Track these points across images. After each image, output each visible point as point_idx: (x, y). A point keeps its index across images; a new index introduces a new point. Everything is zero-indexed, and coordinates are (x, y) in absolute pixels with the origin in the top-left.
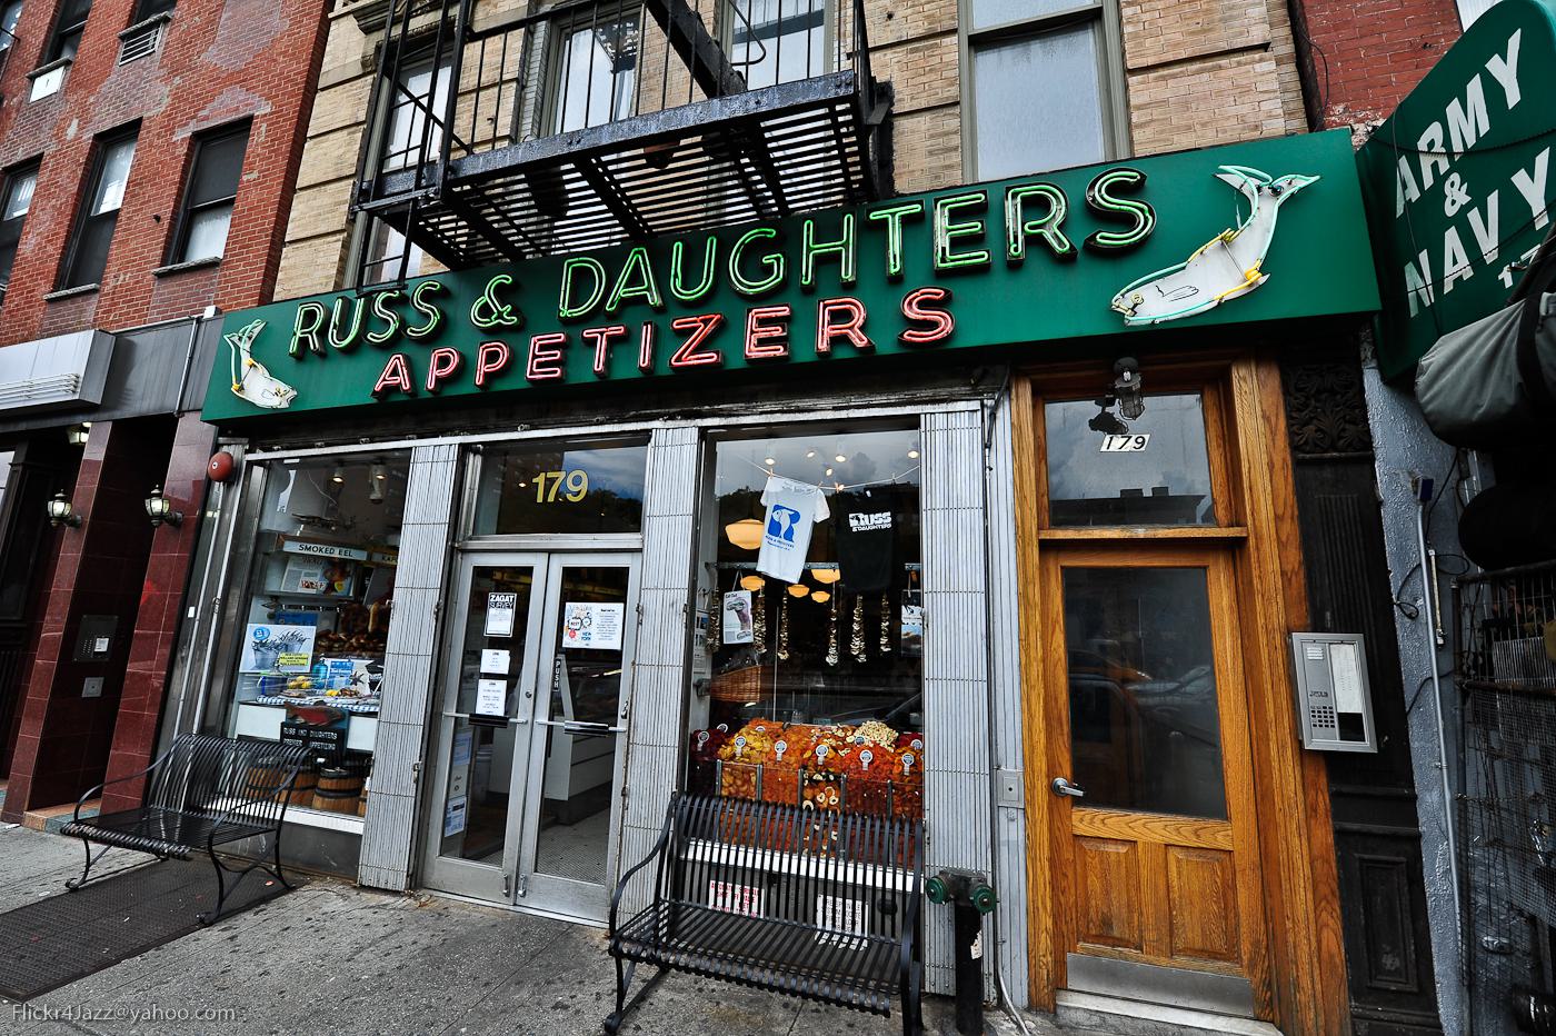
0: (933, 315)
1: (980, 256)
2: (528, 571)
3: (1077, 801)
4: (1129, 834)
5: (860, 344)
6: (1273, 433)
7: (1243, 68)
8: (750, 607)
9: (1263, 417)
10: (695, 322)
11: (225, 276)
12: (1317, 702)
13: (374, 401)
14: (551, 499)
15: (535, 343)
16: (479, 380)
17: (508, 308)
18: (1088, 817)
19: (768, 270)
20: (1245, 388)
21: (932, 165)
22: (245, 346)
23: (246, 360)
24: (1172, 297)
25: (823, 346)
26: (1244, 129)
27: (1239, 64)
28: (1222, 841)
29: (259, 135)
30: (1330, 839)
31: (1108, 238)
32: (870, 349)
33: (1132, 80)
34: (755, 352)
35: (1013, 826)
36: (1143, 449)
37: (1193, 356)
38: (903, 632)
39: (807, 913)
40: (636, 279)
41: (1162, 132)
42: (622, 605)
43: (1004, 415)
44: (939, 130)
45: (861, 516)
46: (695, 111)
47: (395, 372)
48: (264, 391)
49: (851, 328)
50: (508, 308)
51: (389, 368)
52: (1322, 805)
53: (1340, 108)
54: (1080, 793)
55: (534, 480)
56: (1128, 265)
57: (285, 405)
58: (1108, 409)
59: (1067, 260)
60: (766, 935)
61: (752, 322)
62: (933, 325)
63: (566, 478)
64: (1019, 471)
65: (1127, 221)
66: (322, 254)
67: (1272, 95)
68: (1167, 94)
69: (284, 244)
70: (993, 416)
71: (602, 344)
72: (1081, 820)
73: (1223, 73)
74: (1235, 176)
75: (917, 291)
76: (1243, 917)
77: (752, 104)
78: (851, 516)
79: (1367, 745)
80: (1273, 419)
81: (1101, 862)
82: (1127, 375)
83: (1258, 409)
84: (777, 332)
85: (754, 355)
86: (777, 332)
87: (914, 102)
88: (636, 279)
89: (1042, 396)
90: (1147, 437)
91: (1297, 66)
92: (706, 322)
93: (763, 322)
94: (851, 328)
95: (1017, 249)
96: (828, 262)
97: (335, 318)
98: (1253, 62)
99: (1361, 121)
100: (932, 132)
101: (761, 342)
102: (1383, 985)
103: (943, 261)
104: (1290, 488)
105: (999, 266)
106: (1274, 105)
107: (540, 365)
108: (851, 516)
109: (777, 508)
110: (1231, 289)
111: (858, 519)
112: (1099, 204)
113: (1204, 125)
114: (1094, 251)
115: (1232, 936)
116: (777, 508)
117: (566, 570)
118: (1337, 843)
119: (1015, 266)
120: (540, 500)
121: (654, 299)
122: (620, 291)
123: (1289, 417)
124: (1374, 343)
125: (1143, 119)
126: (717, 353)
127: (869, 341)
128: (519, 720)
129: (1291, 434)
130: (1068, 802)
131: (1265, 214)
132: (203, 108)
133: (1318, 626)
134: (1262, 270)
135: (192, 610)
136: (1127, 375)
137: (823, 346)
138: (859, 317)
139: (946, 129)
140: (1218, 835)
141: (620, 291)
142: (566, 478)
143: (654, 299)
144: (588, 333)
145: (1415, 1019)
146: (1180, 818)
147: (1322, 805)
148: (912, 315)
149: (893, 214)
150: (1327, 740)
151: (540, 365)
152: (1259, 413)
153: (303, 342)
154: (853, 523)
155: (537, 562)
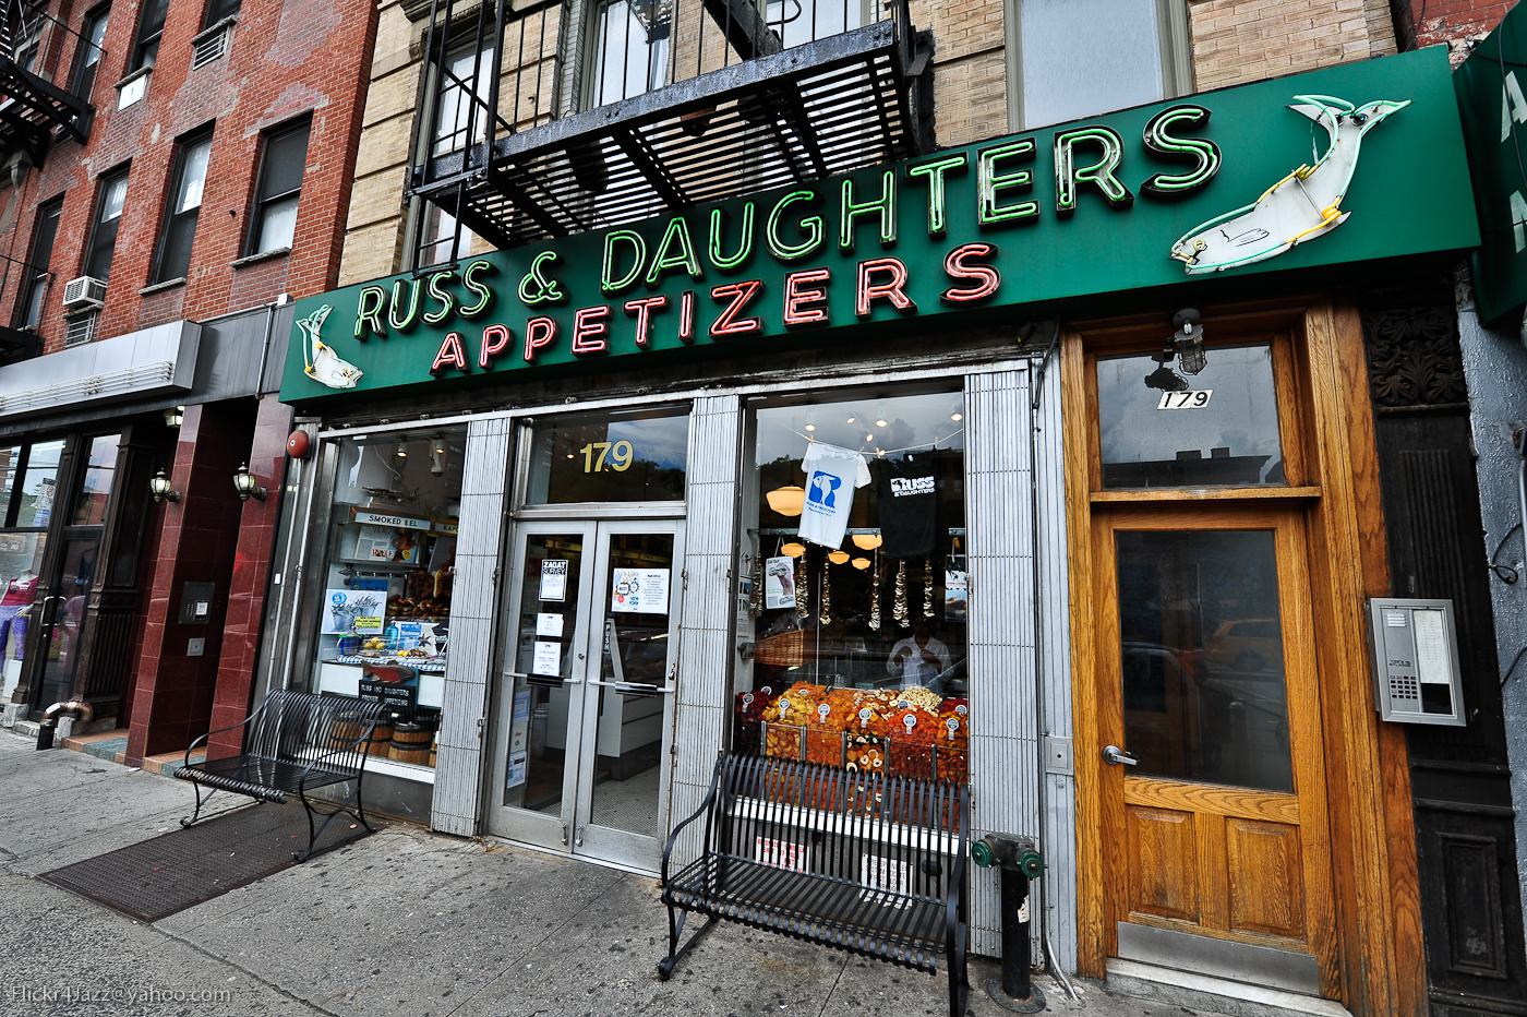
0: (975, 272)
1: (1027, 208)
3: (1129, 770)
4: (1184, 804)
5: (901, 305)
8: (792, 572)
9: (1341, 368)
13: (432, 378)
14: (598, 469)
16: (528, 355)
17: (554, 283)
18: (1142, 786)
20: (1321, 337)
22: (315, 330)
23: (316, 343)
24: (1238, 241)
25: (863, 309)
26: (1323, 53)
29: (319, 127)
30: (1410, 816)
31: (1167, 181)
34: (795, 318)
35: (1062, 792)
36: (1205, 405)
37: (1264, 304)
38: (948, 596)
39: (852, 871)
40: (675, 249)
47: (450, 351)
50: (554, 283)
51: (445, 347)
54: (1133, 762)
55: (582, 451)
56: (1189, 210)
58: (1166, 365)
59: (1122, 207)
61: (791, 288)
62: (977, 282)
63: (612, 448)
64: (1069, 431)
65: (1189, 162)
69: (345, 232)
71: (643, 315)
72: (1134, 789)
75: (961, 247)
76: (1309, 892)
78: (892, 481)
79: (1454, 718)
80: (1352, 370)
82: (1188, 328)
83: (1336, 360)
84: (817, 296)
86: (817, 296)
87: (956, 50)
88: (675, 249)
90: (1209, 393)
92: (745, 289)
93: (802, 287)
95: (1068, 198)
96: (869, 221)
97: (395, 300)
99: (1461, 36)
100: (975, 80)
104: (1371, 444)
107: (585, 339)
109: (818, 474)
111: (900, 484)
112: (1158, 146)
114: (1151, 196)
116: (818, 474)
117: (616, 540)
118: (1416, 820)
119: (1065, 216)
120: (587, 470)
121: (694, 269)
122: (661, 262)
124: (1471, 283)
125: (1207, 51)
127: (910, 302)
132: (269, 106)
133: (1400, 591)
134: (1342, 208)
135: (278, 577)
136: (1188, 328)
137: (863, 309)
139: (990, 75)
140: (1281, 808)
142: (612, 448)
143: (694, 269)
144: (630, 305)
149: (935, 169)
151: (585, 339)
153: (367, 324)
154: (895, 488)
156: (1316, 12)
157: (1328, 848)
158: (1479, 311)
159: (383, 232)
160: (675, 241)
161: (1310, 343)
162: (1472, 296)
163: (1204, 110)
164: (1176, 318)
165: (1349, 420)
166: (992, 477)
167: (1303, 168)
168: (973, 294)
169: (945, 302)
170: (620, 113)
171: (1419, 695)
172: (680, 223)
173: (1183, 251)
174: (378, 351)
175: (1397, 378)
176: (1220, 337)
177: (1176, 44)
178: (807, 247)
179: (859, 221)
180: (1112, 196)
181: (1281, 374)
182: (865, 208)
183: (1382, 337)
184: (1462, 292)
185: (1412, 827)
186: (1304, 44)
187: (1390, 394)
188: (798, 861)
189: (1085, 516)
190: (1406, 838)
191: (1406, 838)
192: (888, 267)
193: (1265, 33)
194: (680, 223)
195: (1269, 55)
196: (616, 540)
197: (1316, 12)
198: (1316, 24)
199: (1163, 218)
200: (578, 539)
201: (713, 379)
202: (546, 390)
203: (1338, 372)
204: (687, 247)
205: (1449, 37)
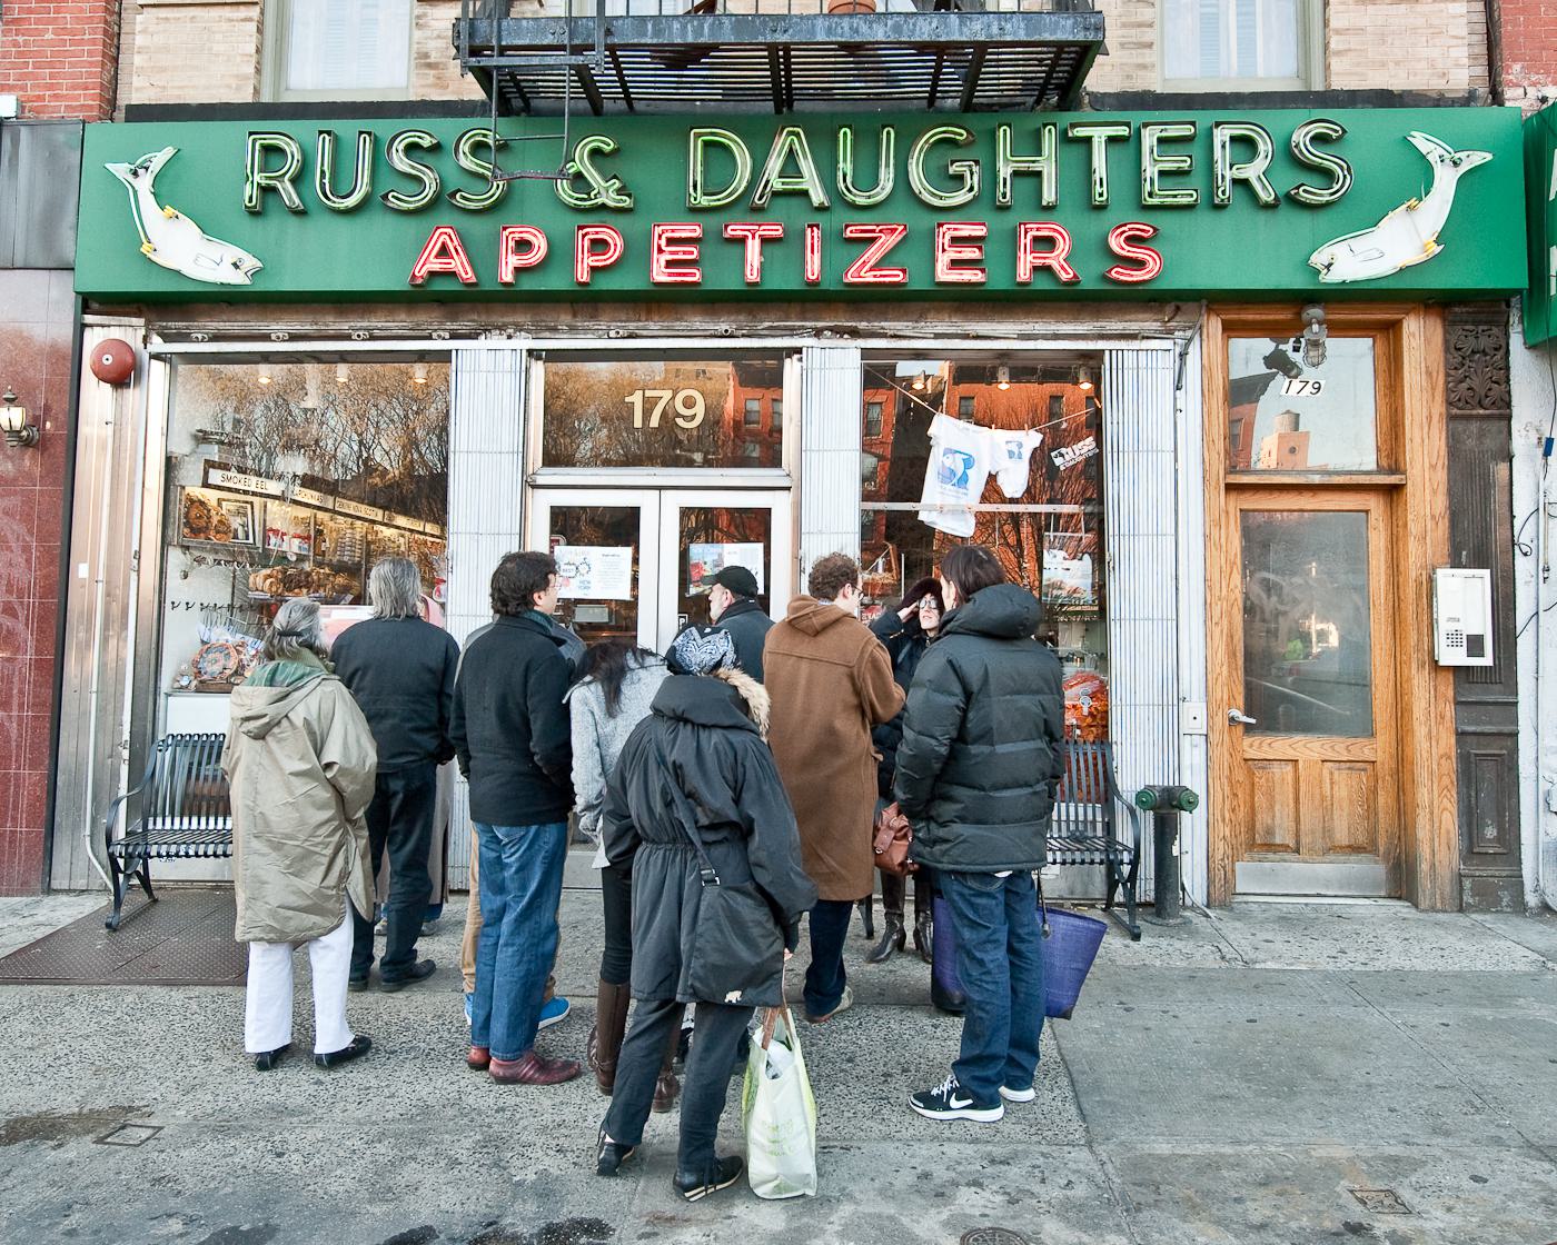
2: (634, 513)
3: (1248, 728)
4: (1291, 754)
5: (1064, 277)
6: (1433, 389)
9: (1427, 372)
10: (873, 231)
11: (16, 44)
12: (1452, 627)
14: (654, 422)
15: (660, 236)
18: (1256, 744)
20: (1414, 344)
21: (1124, 61)
22: (144, 184)
23: (148, 202)
24: (1361, 257)
26: (1433, 74)
28: (1368, 754)
30: (1453, 740)
32: (1075, 281)
34: (944, 274)
35: (1196, 751)
37: (1371, 309)
41: (1358, 64)
42: (760, 547)
43: (1194, 350)
44: (1133, 19)
45: (1063, 450)
46: (930, 24)
47: (444, 252)
48: (191, 253)
52: (1448, 714)
53: (1517, 67)
54: (1253, 721)
56: (1323, 219)
58: (1281, 347)
60: (1095, 765)
62: (1139, 264)
63: (673, 398)
64: (1206, 415)
66: (219, 37)
67: (1460, 42)
70: (1183, 355)
72: (1251, 746)
75: (1125, 225)
76: (1381, 815)
77: (995, 30)
78: (1053, 454)
79: (1487, 660)
80: (1435, 374)
81: (1267, 780)
82: (1315, 327)
83: (1423, 365)
84: (970, 253)
86: (970, 253)
89: (1231, 329)
90: (1322, 383)
99: (1534, 84)
100: (1124, 19)
102: (1484, 850)
103: (1150, 195)
106: (1461, 53)
108: (1053, 454)
110: (1411, 256)
111: (1062, 455)
112: (1301, 151)
113: (1397, 63)
114: (1293, 201)
115: (1373, 841)
117: (685, 512)
118: (1457, 742)
120: (638, 423)
121: (818, 196)
123: (1447, 375)
124: (1522, 310)
125: (1341, 47)
126: (904, 271)
127: (1075, 275)
129: (1448, 391)
130: (1240, 729)
131: (1446, 182)
133: (1456, 563)
136: (1315, 327)
139: (1140, 19)
140: (1363, 749)
143: (818, 196)
144: (734, 230)
145: (1504, 874)
146: (1335, 738)
147: (1448, 714)
148: (1116, 249)
150: (1453, 656)
152: (1423, 369)
154: (1058, 461)
155: (645, 501)
156: (1431, 31)
157: (1395, 777)
158: (1524, 332)
159: (225, 26)
161: (1405, 349)
162: (1521, 320)
163: (1344, 131)
164: (1304, 316)
165: (1430, 418)
166: (491, 380)
167: (1413, 202)
168: (1138, 276)
170: (791, 31)
171: (1465, 644)
172: (798, 135)
173: (1319, 259)
174: (277, 226)
175: (1465, 385)
176: (1338, 329)
178: (961, 197)
181: (1380, 372)
184: (1514, 319)
185: (1454, 749)
186: (1419, 60)
187: (1459, 400)
190: (1449, 758)
191: (1449, 758)
192: (1051, 234)
194: (798, 135)
195: (1391, 65)
196: (685, 512)
197: (1431, 31)
198: (1431, 42)
199: (1304, 220)
200: (634, 513)
201: (820, 324)
202: (575, 316)
203: (1424, 376)
204: (807, 165)
205: (1526, 84)
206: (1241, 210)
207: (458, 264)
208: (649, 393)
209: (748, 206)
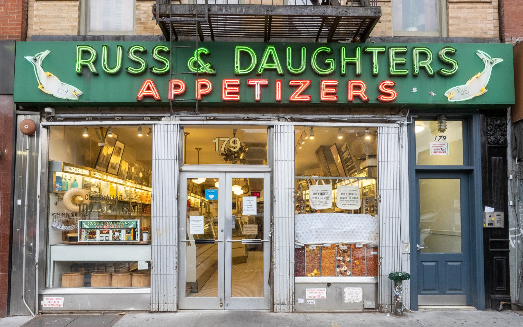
1: (404, 71)
7: (484, 10)
19: (328, 66)
22: (39, 63)
25: (351, 98)
27: (483, 8)
31: (445, 71)
33: (450, 6)
34: (324, 98)
37: (464, 112)
39: (341, 295)
40: (271, 60)
47: (148, 88)
49: (361, 93)
51: (145, 86)
56: (448, 81)
57: (76, 98)
59: (432, 76)
62: (389, 95)
65: (450, 66)
68: (460, 15)
73: (478, 10)
74: (481, 54)
84: (333, 90)
85: (322, 99)
86: (333, 90)
91: (498, 10)
92: (305, 83)
94: (361, 93)
95: (417, 71)
98: (486, 8)
101: (327, 94)
105: (410, 74)
113: (471, 29)
119: (415, 76)
121: (280, 71)
122: (265, 65)
128: (219, 240)
131: (488, 69)
134: (486, 88)
137: (351, 98)
138: (363, 89)
141: (265, 65)
153: (84, 67)
160: (271, 56)
169: (377, 100)
177: (442, 18)
178: (328, 71)
179: (348, 64)
180: (430, 73)
182: (350, 60)
183: (490, 125)
188: (323, 293)
189: (414, 172)
193: (468, 21)
194: (272, 49)
204: (276, 59)
206: (422, 78)
207: (154, 93)
208: (220, 139)
209: (254, 74)
